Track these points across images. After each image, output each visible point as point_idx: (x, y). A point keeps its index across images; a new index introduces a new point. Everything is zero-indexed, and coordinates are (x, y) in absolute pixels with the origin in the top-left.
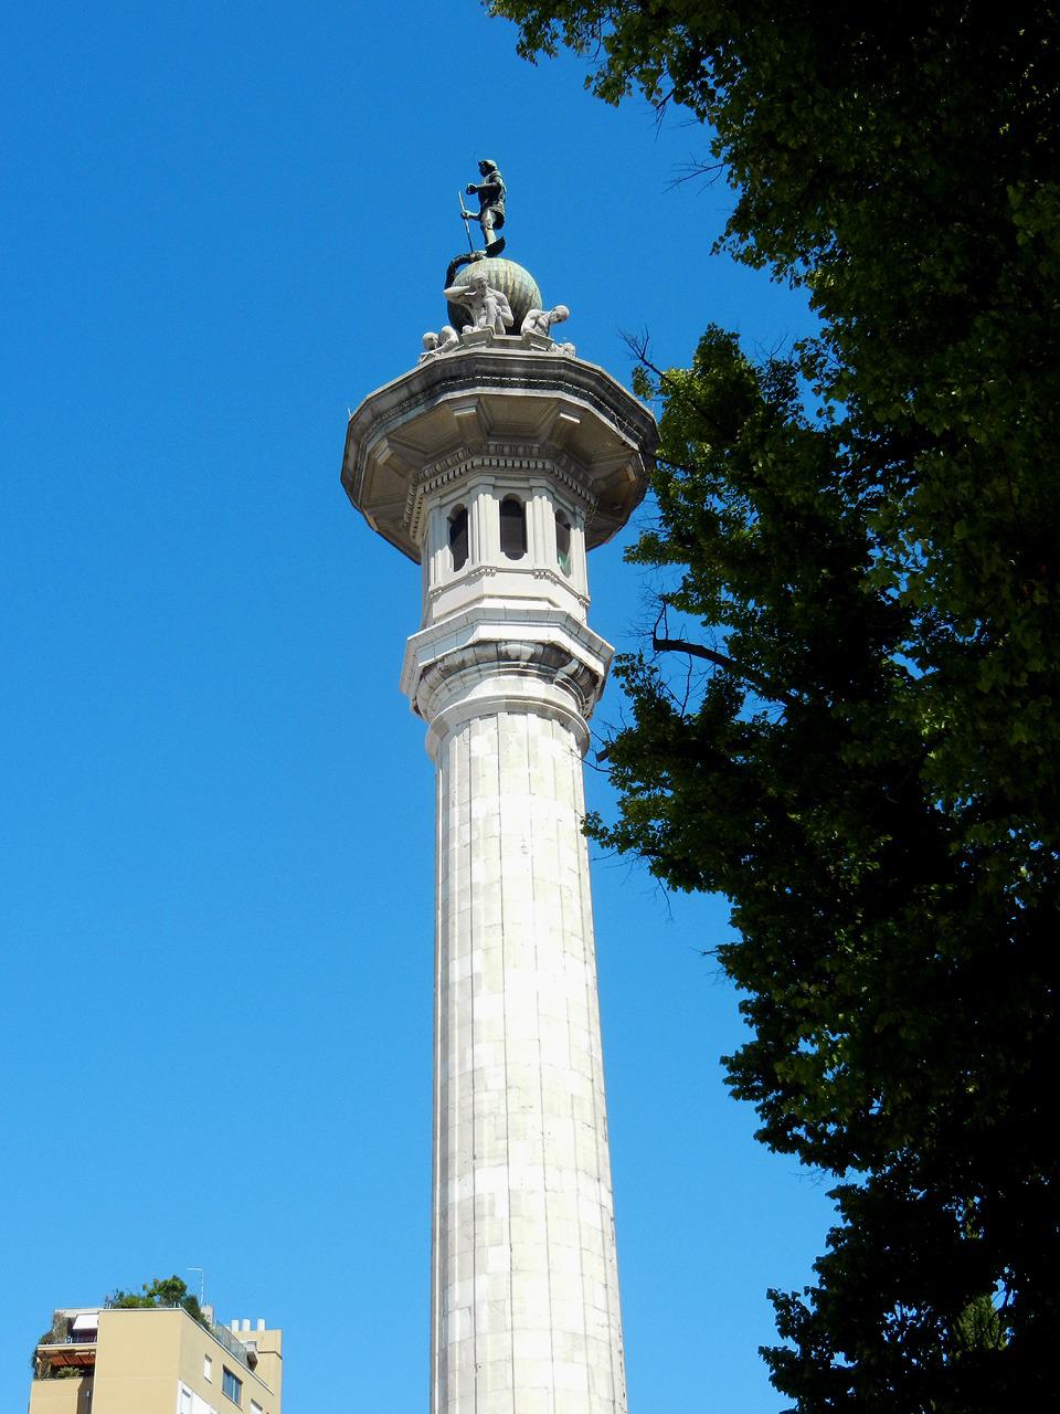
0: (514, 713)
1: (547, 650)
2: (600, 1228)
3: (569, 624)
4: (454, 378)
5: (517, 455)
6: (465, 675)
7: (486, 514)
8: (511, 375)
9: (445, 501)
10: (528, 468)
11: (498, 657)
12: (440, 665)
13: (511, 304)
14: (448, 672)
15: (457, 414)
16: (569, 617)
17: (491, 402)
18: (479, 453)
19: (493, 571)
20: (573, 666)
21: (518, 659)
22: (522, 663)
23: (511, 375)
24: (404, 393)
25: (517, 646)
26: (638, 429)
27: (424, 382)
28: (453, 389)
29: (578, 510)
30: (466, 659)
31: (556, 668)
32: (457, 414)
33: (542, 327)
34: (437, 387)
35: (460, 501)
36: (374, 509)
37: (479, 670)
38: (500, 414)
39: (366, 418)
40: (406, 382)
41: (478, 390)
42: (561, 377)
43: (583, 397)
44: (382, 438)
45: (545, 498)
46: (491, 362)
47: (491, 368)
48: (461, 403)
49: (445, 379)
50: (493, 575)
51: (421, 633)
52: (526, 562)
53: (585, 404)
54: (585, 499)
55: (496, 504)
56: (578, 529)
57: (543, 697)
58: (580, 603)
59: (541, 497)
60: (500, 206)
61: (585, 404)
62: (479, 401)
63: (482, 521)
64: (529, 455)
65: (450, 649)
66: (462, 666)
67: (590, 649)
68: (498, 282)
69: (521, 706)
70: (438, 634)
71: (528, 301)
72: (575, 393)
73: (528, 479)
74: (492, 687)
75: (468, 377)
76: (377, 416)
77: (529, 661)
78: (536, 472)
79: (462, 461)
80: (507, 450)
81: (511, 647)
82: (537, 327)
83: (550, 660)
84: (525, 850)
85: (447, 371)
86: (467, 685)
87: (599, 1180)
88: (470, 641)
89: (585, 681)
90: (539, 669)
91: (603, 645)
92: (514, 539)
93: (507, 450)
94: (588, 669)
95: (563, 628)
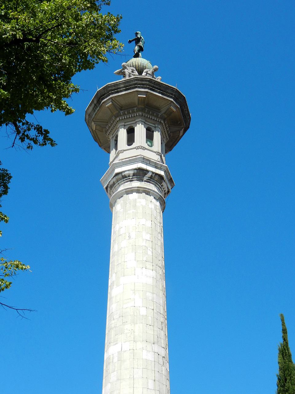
0: (128, 194)
1: (138, 171)
4: (104, 95)
6: (115, 187)
7: (122, 134)
8: (120, 88)
10: (134, 116)
12: (109, 186)
13: (136, 70)
14: (112, 187)
15: (106, 106)
17: (117, 99)
20: (149, 174)
21: (129, 176)
23: (120, 88)
24: (93, 105)
29: (156, 125)
30: (114, 181)
31: (144, 176)
32: (106, 106)
33: (149, 74)
34: (100, 100)
38: (123, 102)
40: (93, 101)
41: (111, 96)
42: (136, 84)
45: (140, 124)
46: (113, 86)
47: (113, 88)
48: (107, 102)
49: (101, 96)
50: (123, 152)
53: (146, 90)
54: (158, 121)
56: (157, 132)
58: (157, 154)
59: (139, 124)
60: (141, 44)
61: (146, 90)
62: (112, 100)
64: (133, 112)
66: (114, 184)
67: (156, 167)
70: (107, 176)
72: (142, 88)
73: (135, 120)
75: (108, 93)
76: (89, 115)
78: (137, 117)
80: (126, 112)
81: (126, 173)
82: (148, 75)
83: (140, 174)
84: (130, 237)
87: (154, 343)
89: (157, 178)
90: (137, 178)
92: (131, 140)
93: (126, 112)
94: (156, 174)
95: (143, 162)
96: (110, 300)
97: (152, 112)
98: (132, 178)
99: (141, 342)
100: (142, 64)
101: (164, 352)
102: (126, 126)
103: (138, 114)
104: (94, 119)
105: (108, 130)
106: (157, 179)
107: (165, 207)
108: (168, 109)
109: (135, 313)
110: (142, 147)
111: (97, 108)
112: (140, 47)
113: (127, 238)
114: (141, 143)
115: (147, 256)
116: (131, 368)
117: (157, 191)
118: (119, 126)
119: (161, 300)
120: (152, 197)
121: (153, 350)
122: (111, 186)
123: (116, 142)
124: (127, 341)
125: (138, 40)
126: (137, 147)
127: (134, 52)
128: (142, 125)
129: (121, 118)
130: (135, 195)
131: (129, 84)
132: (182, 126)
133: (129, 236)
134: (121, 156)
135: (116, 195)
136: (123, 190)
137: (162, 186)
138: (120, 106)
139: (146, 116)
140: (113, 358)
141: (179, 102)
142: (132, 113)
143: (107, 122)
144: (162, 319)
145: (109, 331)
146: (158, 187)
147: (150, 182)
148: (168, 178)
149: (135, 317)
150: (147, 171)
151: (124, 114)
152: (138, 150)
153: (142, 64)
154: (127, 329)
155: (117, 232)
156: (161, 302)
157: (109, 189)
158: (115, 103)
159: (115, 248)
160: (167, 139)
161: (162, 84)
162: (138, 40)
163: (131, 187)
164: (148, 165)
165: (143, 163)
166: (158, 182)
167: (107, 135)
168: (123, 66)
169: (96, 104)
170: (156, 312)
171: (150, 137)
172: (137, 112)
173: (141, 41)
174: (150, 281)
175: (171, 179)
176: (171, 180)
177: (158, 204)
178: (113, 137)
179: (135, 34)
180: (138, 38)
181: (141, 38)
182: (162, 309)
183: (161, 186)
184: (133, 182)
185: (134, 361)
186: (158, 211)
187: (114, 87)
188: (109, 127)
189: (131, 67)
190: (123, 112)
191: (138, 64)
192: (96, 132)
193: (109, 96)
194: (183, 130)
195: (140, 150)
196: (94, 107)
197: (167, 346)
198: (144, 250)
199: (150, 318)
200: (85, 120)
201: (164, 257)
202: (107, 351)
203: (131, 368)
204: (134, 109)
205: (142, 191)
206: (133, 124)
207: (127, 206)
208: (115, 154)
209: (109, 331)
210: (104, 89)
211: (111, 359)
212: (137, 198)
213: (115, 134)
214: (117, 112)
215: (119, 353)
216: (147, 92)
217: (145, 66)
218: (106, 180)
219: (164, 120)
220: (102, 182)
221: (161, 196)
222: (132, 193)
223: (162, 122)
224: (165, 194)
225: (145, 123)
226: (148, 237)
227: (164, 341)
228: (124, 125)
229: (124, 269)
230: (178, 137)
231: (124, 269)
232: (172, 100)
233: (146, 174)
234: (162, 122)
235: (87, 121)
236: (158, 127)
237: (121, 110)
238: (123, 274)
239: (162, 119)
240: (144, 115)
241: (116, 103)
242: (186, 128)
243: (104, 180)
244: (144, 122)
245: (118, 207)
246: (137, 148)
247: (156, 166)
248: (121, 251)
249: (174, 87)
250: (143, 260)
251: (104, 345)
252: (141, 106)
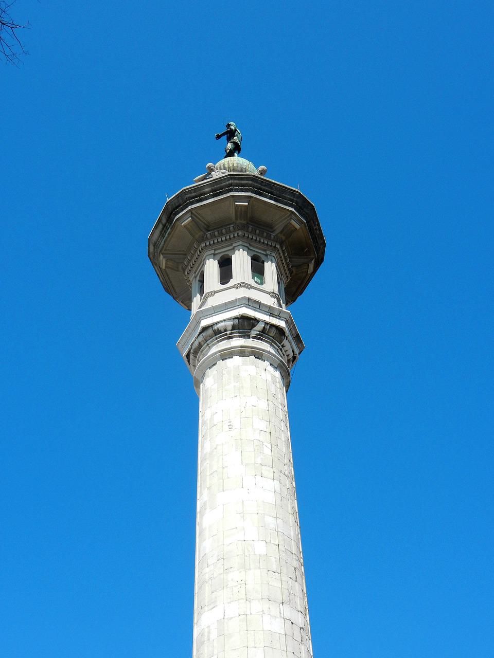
0: (226, 359)
1: (241, 320)
2: (283, 632)
4: (177, 207)
6: (203, 351)
7: (211, 268)
8: (205, 194)
14: (196, 352)
18: (203, 241)
20: (260, 326)
21: (226, 330)
23: (205, 194)
24: (161, 226)
26: (292, 200)
29: (268, 252)
31: (251, 330)
34: (172, 216)
38: (210, 217)
41: (190, 207)
42: (231, 185)
45: (241, 250)
46: (193, 191)
47: (193, 194)
48: (184, 218)
49: (174, 210)
53: (249, 194)
54: (271, 246)
56: (270, 262)
58: (271, 296)
59: (239, 250)
60: (236, 139)
61: (249, 194)
62: (192, 213)
66: (200, 346)
67: (271, 315)
68: (224, 167)
70: (187, 335)
76: (155, 245)
77: (232, 330)
80: (216, 233)
83: (244, 325)
84: (230, 427)
89: (273, 332)
90: (239, 333)
93: (216, 233)
94: (272, 326)
95: (248, 306)
96: (199, 535)
97: (260, 231)
98: (231, 333)
99: (259, 601)
100: (239, 166)
101: (302, 620)
103: (236, 235)
104: (164, 249)
105: (187, 266)
106: (274, 334)
107: (290, 381)
108: (286, 226)
109: (246, 550)
110: (245, 284)
111: (168, 230)
112: (235, 144)
113: (226, 428)
114: (243, 278)
115: (262, 457)
116: (244, 647)
117: (274, 353)
118: (206, 254)
119: (292, 530)
120: (267, 363)
121: (283, 616)
122: (196, 351)
123: (201, 284)
124: (233, 601)
125: (231, 134)
126: (237, 284)
127: (226, 151)
129: (208, 244)
130: (237, 359)
131: (218, 186)
132: (312, 256)
133: (230, 425)
134: (212, 302)
135: (204, 362)
136: (215, 353)
137: (283, 346)
138: (205, 224)
139: (250, 237)
140: (209, 633)
141: (304, 214)
142: (227, 233)
143: (185, 255)
144: (296, 564)
145: (200, 588)
146: (276, 349)
147: (261, 339)
148: (292, 335)
149: (246, 558)
151: (213, 236)
152: (238, 289)
153: (239, 166)
154: (232, 580)
155: (208, 422)
156: (292, 534)
157: (191, 356)
158: (197, 220)
159: (205, 447)
160: (287, 277)
161: (274, 183)
162: (231, 134)
163: (229, 346)
164: (258, 311)
165: (249, 308)
166: (276, 339)
167: (186, 274)
168: (209, 168)
169: (166, 224)
170: (284, 550)
171: (258, 269)
172: (235, 231)
173: (237, 136)
174: (270, 498)
175: (298, 335)
176: (297, 338)
177: (277, 374)
178: (196, 277)
179: (227, 126)
180: (231, 130)
181: (236, 130)
182: (295, 545)
183: (281, 347)
184: (233, 339)
185: (248, 635)
186: (278, 385)
187: (195, 192)
188: (189, 261)
189: (221, 170)
190: (210, 234)
191: (233, 165)
192: (166, 272)
194: (313, 262)
195: (242, 289)
196: (163, 229)
197: (307, 611)
198: (257, 446)
199: (274, 559)
200: (149, 256)
201: (292, 462)
202: (197, 622)
203: (244, 647)
204: (229, 228)
205: (249, 352)
206: (229, 252)
207: (224, 378)
208: (201, 299)
209: (200, 588)
210: (178, 197)
211: (206, 634)
212: (240, 364)
213: (199, 271)
214: (201, 233)
215: (221, 622)
216: (251, 197)
218: (186, 341)
219: (281, 244)
220: (180, 346)
221: (281, 361)
222: (232, 357)
223: (278, 246)
224: (289, 361)
225: (249, 249)
226: (263, 425)
227: (301, 602)
228: (214, 255)
229: (223, 480)
230: (305, 277)
231: (223, 480)
232: (293, 210)
234: (278, 246)
235: (151, 256)
236: (271, 255)
237: (208, 231)
238: (222, 488)
239: (277, 242)
240: (246, 235)
241: (199, 219)
242: (319, 262)
243: (182, 343)
244: (247, 247)
245: (211, 384)
246: (237, 286)
247: (270, 312)
248: (216, 452)
249: (294, 189)
250: (257, 462)
251: (198, 432)
252: (241, 221)
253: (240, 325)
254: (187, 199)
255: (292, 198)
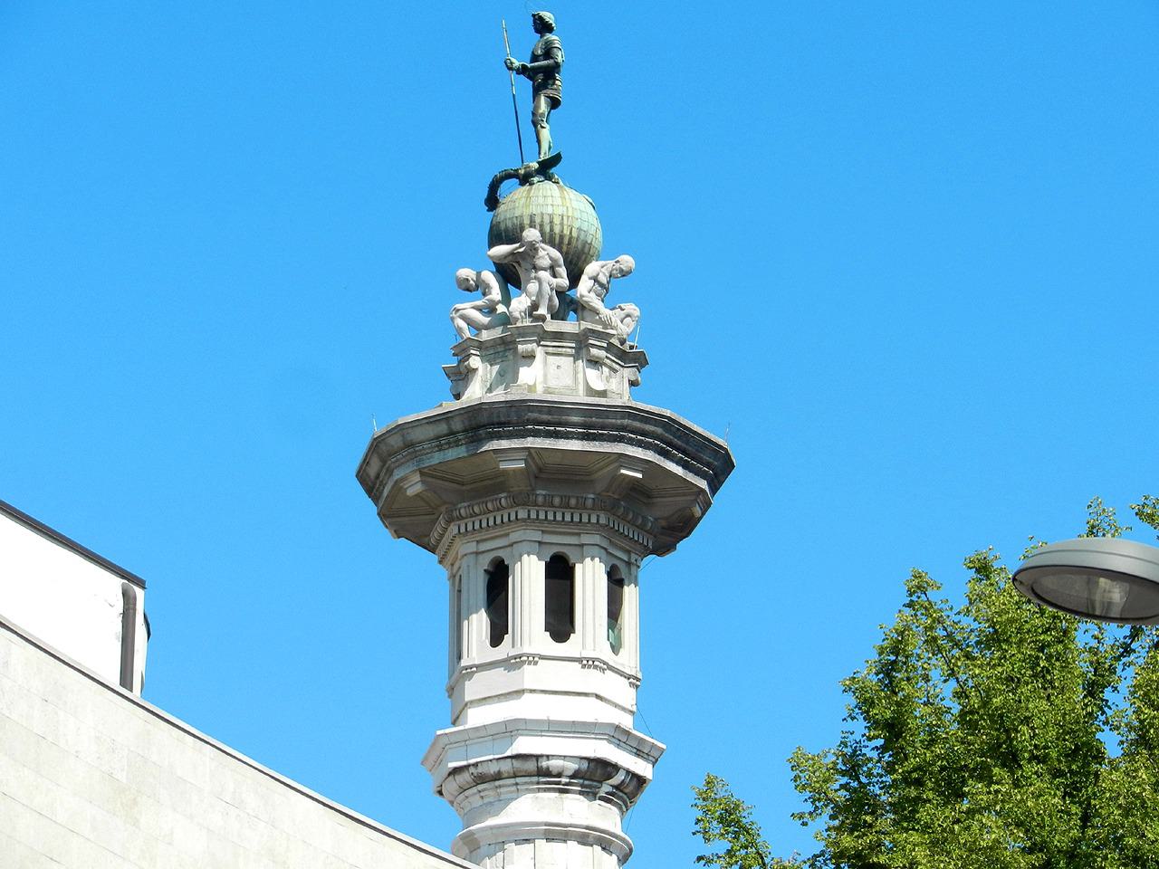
1: (592, 765)
3: (619, 736)
4: (501, 424)
5: (568, 506)
6: (500, 786)
7: (529, 578)
9: (483, 547)
11: (539, 773)
12: (472, 770)
14: (481, 779)
16: (618, 727)
19: (534, 659)
21: (559, 775)
22: (564, 780)
24: (443, 428)
25: (559, 763)
27: (467, 423)
28: (499, 437)
31: (601, 782)
35: (500, 553)
36: (394, 520)
37: (517, 784)
39: (395, 441)
41: (530, 442)
42: (624, 428)
43: (646, 446)
44: (414, 471)
45: (597, 560)
47: (545, 417)
48: (510, 452)
49: (493, 424)
50: (536, 663)
51: (447, 731)
52: (571, 647)
55: (543, 564)
57: (585, 823)
62: (530, 454)
63: (526, 628)
64: (582, 506)
65: (483, 756)
66: (498, 776)
69: (560, 833)
71: (586, 251)
72: (640, 444)
74: (530, 807)
77: (572, 777)
79: (505, 508)
80: (557, 501)
85: (495, 415)
86: (502, 797)
88: (508, 753)
90: (582, 786)
91: (653, 746)
92: (561, 620)
93: (557, 501)
94: (634, 776)
98: (566, 784)
102: (548, 546)
128: (602, 564)
150: (616, 768)
191: (571, 233)
193: (524, 437)
217: (589, 242)
222: (565, 841)
233: (610, 777)
253: (588, 773)
254: (529, 422)
255: (711, 460)
